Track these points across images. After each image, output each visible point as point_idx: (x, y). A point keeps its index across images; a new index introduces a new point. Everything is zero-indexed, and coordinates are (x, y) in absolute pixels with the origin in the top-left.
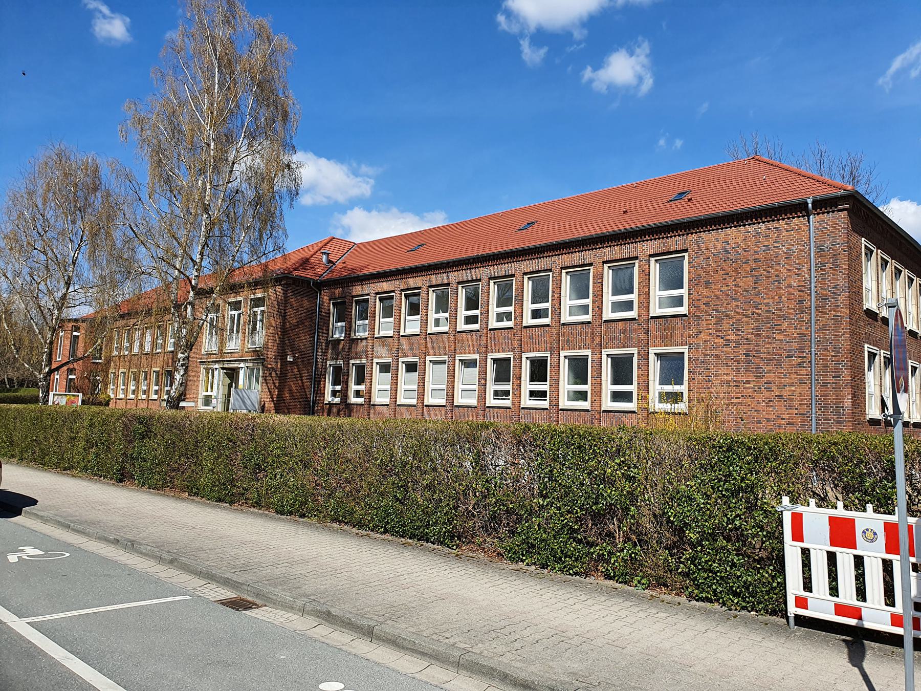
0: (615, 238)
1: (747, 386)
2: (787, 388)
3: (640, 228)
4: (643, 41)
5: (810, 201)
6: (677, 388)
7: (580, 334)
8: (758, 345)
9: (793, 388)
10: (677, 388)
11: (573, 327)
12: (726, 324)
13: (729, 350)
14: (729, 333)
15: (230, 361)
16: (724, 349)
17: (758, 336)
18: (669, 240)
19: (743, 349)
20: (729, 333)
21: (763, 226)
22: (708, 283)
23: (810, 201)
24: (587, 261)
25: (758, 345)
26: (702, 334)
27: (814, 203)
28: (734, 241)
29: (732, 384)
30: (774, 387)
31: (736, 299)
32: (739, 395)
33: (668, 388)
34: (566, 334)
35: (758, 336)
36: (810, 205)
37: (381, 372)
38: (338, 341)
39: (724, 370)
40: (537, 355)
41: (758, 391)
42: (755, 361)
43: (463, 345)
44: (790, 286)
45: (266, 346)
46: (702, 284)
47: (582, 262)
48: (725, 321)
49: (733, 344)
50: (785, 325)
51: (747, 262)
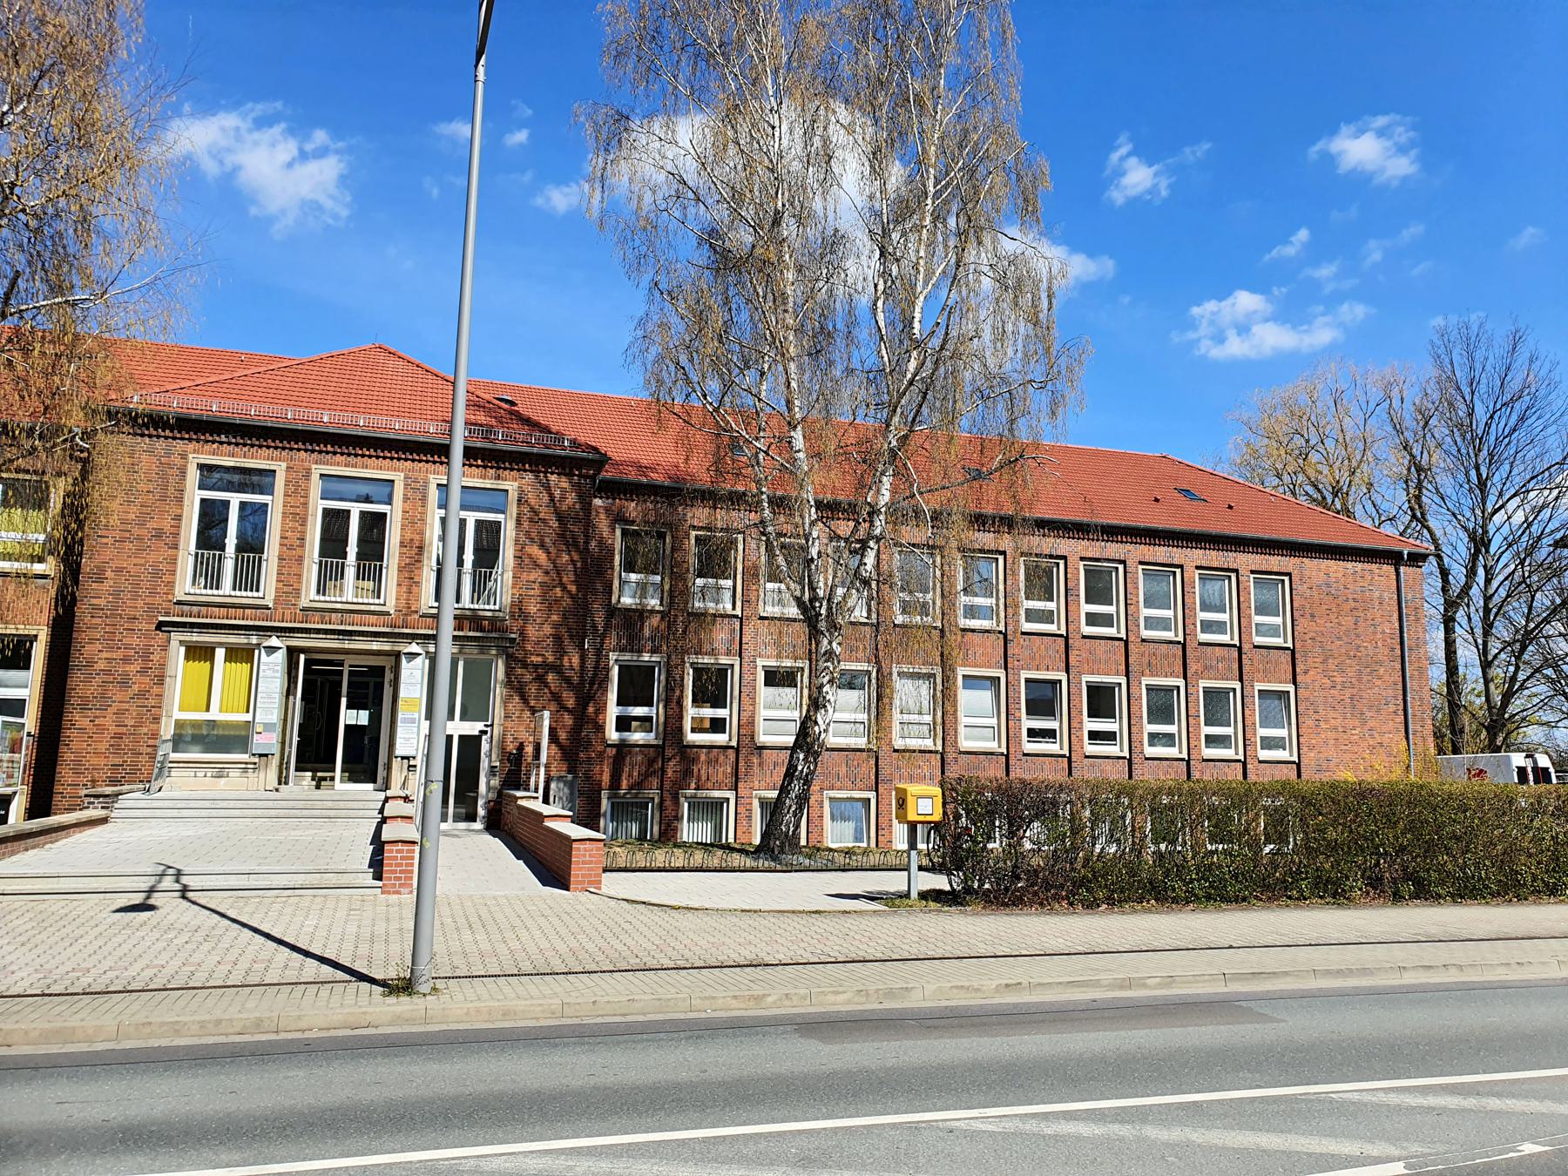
0: (235, 432)
1: (1354, 732)
2: (1387, 735)
3: (209, 419)
4: (548, 199)
5: (1406, 552)
6: (721, 713)
7: (1166, 657)
8: (1360, 689)
9: (1391, 736)
10: (721, 713)
11: (1156, 645)
12: (1332, 663)
13: (1336, 692)
14: (1335, 674)
15: (351, 633)
16: (1332, 692)
17: (1360, 680)
18: (1271, 558)
19: (1348, 693)
20: (1335, 674)
21: (1360, 565)
22: (1312, 616)
23: (1406, 552)
24: (1176, 561)
25: (1360, 689)
26: (1311, 673)
27: (1409, 554)
28: (1335, 575)
29: (1341, 729)
30: (1376, 735)
31: (1339, 638)
32: (1347, 742)
33: (708, 712)
34: (1147, 655)
35: (1360, 680)
36: (1406, 557)
37: (187, 658)
38: (641, 614)
39: (1332, 714)
40: (1104, 680)
41: (1362, 738)
42: (1359, 706)
43: (970, 652)
44: (1383, 632)
45: (519, 609)
46: (1308, 616)
47: (1169, 561)
48: (1330, 661)
49: (1339, 687)
50: (1382, 670)
51: (1347, 600)
